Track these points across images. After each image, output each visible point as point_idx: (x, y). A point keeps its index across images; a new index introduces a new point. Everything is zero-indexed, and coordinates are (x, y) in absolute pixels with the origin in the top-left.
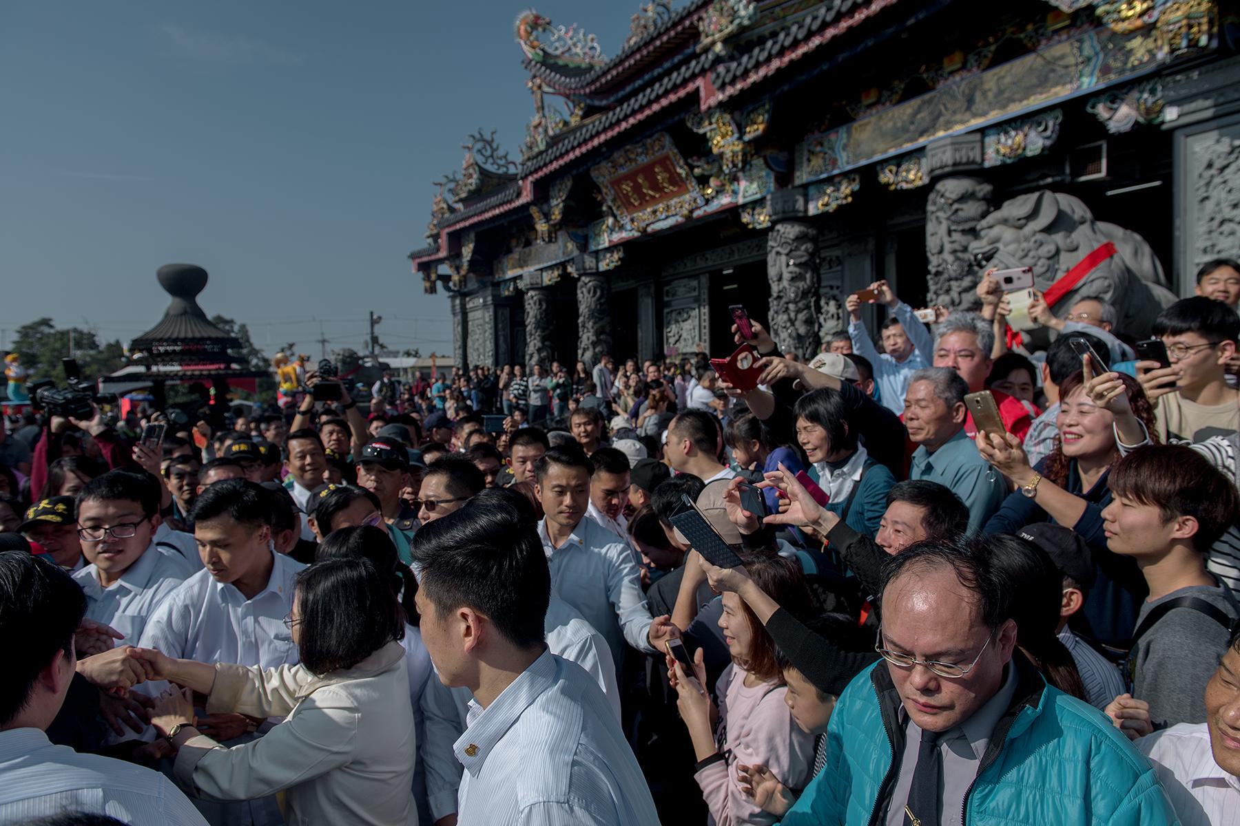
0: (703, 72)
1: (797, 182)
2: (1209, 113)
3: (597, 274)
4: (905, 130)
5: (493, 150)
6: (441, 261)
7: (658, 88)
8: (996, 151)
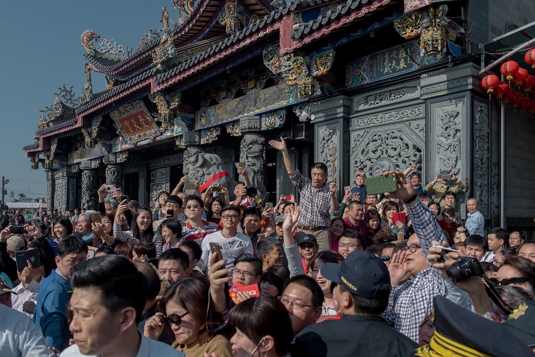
0: (152, 76)
1: (196, 129)
2: (323, 119)
3: (116, 164)
4: (234, 111)
5: (71, 96)
6: (40, 152)
7: (134, 81)
8: (266, 123)
